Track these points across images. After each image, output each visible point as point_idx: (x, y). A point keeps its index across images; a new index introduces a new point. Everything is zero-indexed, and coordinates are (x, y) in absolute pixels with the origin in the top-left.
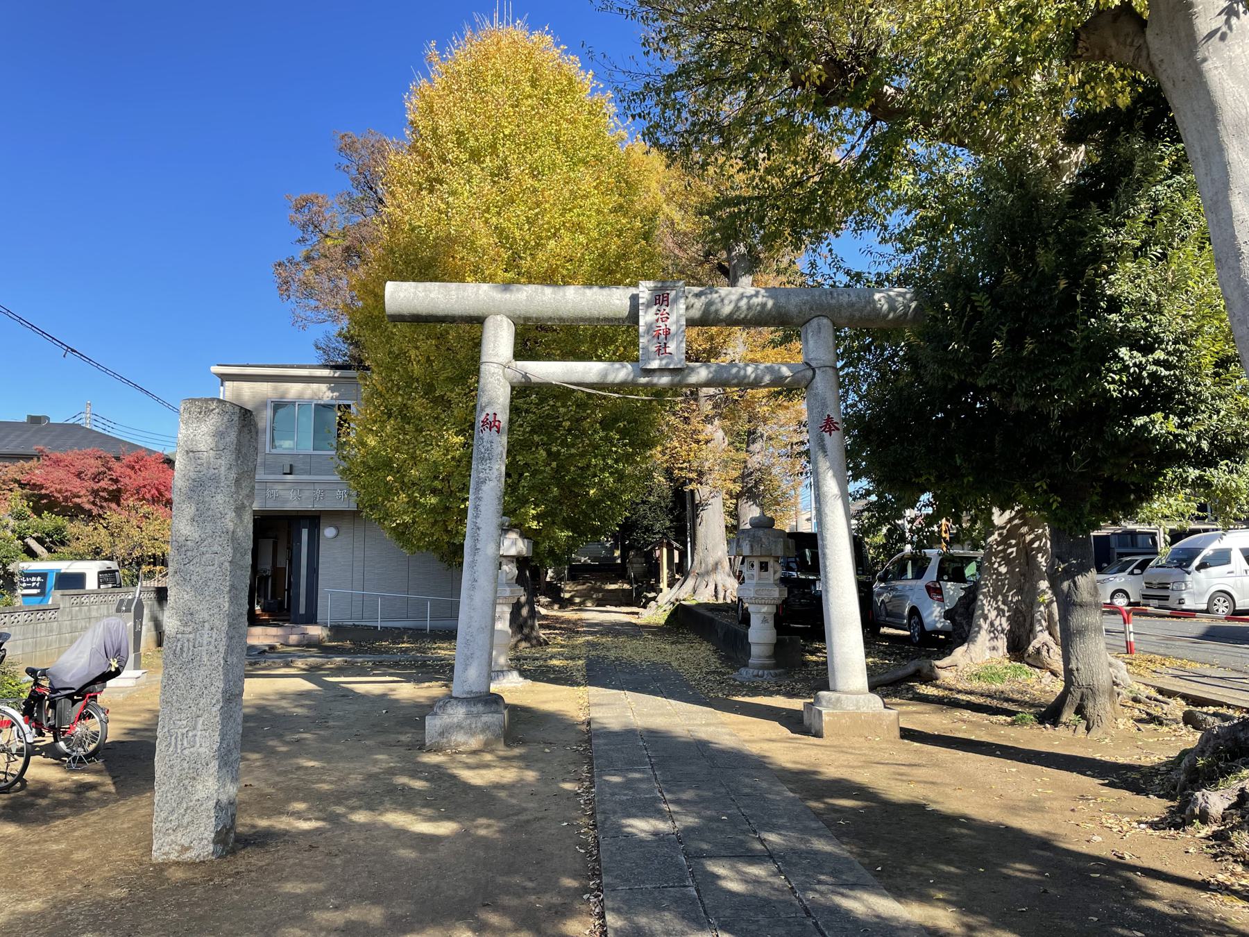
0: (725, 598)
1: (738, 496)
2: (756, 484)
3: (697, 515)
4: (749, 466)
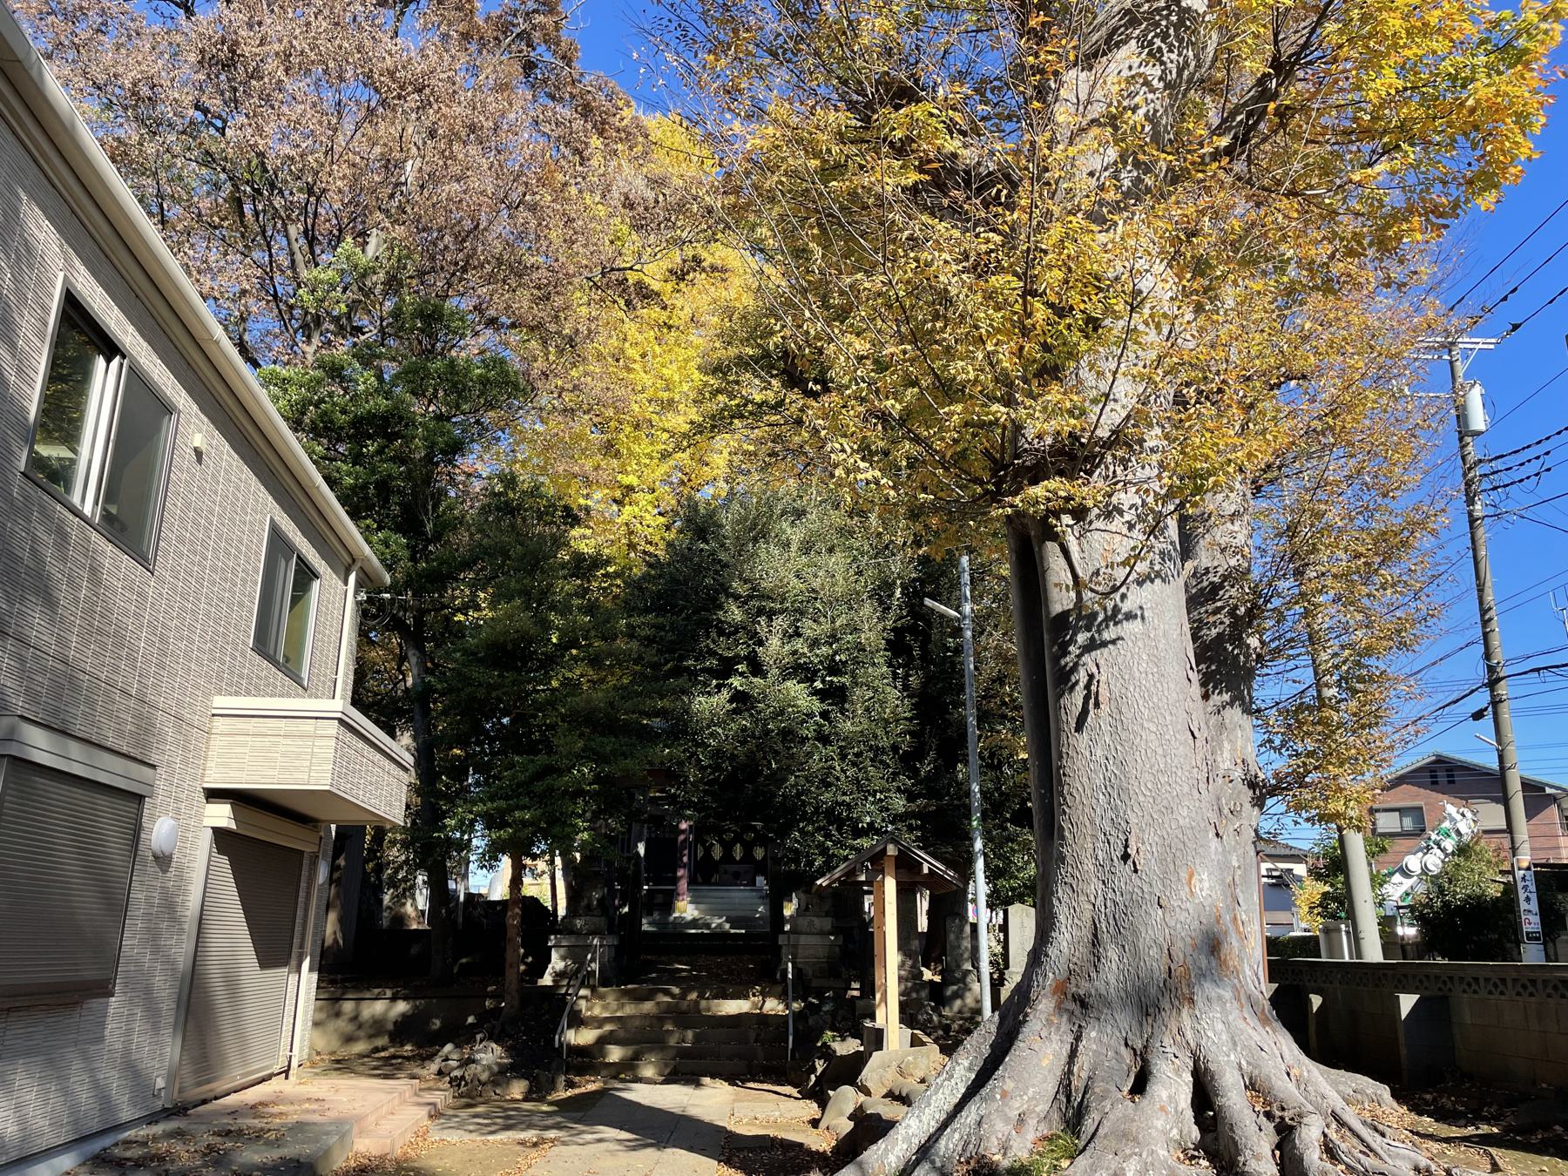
3: (1064, 679)
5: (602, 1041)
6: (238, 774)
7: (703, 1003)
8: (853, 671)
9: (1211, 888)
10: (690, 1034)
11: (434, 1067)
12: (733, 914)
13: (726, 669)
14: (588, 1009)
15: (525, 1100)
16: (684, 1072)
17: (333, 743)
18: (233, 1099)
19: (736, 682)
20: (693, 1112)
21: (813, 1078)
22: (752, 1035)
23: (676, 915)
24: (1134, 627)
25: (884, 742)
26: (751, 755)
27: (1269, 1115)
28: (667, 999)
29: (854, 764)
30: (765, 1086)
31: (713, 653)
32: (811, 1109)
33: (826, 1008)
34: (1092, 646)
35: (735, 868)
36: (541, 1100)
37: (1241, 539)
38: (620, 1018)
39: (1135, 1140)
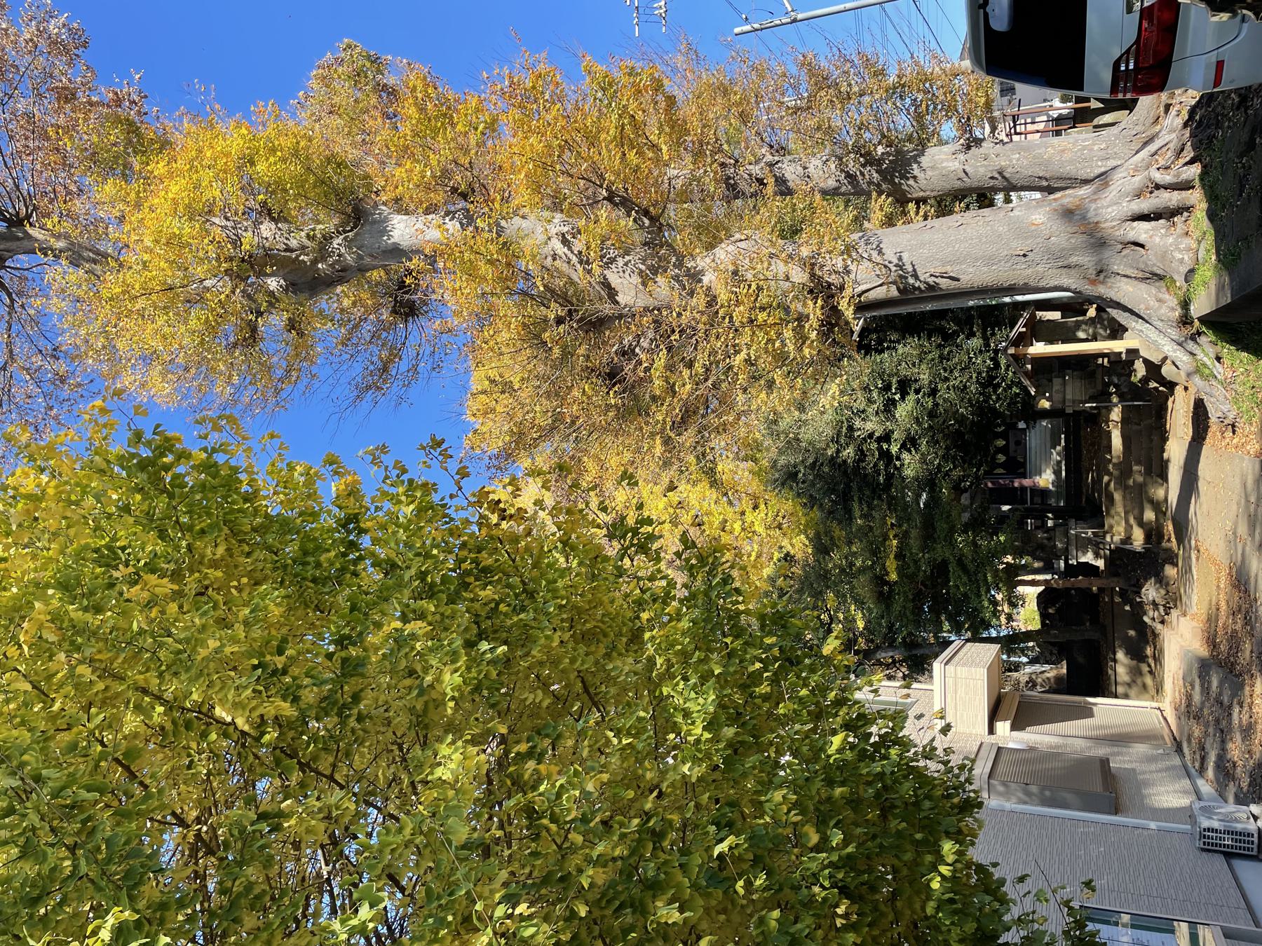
0: (1186, 186)
1: (901, 200)
2: (870, 160)
3: (931, 288)
4: (831, 183)
5: (1141, 524)
6: (979, 718)
7: (1114, 460)
8: (889, 375)
9: (1039, 214)
10: (1135, 468)
11: (1159, 626)
12: (1048, 445)
13: (886, 456)
14: (1120, 534)
15: (1177, 565)
16: (1159, 470)
17: (959, 668)
18: (1174, 728)
19: (894, 449)
20: (1182, 462)
21: (1161, 389)
22: (1135, 427)
23: (1051, 487)
24: (905, 256)
25: (935, 354)
26: (946, 437)
27: (1151, 193)
28: (1112, 484)
29: (951, 372)
30: (1168, 418)
31: (875, 465)
32: (1179, 390)
33: (1116, 381)
34: (916, 277)
35: (1012, 446)
36: (1177, 556)
37: (819, 163)
38: (1126, 513)
39: (1165, 252)
